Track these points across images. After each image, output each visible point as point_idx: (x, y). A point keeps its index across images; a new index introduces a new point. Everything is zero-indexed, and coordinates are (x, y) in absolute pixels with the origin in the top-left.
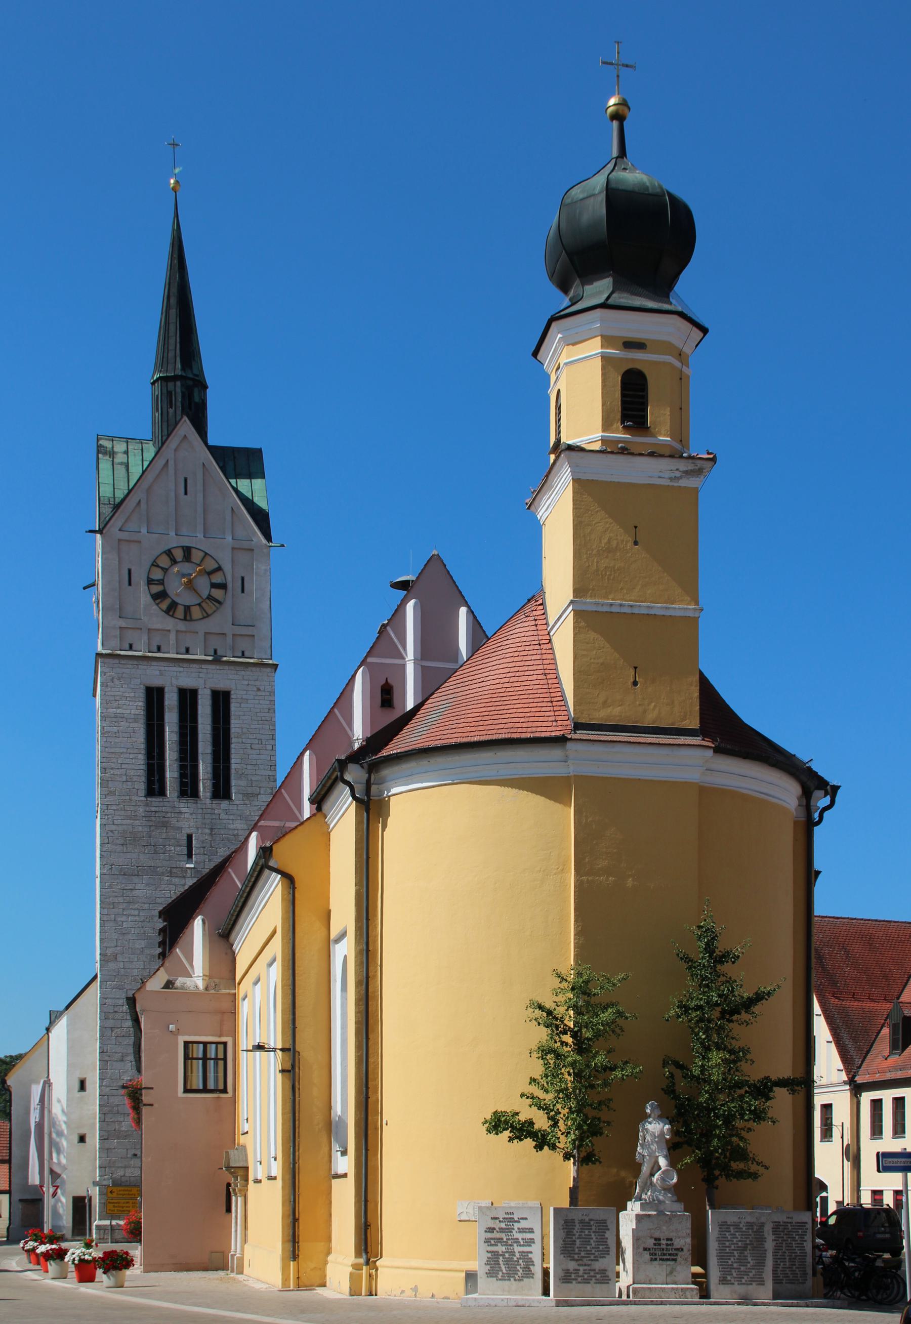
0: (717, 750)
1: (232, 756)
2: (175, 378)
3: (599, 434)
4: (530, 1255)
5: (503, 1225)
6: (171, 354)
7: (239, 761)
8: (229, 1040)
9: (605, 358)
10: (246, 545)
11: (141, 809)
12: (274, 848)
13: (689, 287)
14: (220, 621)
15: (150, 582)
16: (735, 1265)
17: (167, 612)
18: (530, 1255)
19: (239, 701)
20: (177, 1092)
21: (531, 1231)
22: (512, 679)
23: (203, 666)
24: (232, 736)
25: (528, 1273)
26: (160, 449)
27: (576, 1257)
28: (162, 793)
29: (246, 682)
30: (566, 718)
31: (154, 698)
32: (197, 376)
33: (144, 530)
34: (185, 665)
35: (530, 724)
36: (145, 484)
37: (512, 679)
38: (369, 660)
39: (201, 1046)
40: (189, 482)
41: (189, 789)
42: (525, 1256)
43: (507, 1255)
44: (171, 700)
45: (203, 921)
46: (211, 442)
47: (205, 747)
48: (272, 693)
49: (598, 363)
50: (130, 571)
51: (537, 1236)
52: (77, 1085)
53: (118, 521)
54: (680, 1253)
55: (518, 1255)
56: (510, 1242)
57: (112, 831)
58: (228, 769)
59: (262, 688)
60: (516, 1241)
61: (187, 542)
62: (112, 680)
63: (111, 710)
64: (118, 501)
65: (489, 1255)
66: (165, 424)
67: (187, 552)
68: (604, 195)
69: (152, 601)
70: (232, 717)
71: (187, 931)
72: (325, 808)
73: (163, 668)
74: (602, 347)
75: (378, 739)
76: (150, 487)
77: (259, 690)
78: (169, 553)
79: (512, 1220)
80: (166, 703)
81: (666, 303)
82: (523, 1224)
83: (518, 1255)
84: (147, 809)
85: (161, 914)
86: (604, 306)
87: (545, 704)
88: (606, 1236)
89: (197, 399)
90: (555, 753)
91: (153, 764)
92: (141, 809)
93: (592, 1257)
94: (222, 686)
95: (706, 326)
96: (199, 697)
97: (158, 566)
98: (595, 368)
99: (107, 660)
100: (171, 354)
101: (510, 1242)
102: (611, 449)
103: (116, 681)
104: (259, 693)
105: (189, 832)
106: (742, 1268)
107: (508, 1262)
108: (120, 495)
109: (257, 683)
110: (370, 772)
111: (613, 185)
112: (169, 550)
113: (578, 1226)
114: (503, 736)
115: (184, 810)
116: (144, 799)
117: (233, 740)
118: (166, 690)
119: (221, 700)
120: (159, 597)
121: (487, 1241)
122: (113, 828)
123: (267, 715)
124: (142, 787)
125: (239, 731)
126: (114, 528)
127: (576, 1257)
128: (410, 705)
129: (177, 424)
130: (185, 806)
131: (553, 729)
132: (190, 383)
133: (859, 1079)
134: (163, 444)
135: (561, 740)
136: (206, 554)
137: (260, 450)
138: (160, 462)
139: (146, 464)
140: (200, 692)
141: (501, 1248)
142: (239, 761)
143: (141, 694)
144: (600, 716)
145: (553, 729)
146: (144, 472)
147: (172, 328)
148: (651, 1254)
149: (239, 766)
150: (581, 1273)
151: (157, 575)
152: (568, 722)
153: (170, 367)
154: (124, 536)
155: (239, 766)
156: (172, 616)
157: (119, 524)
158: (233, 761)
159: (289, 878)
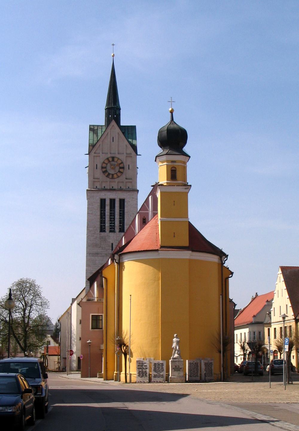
1: (125, 219)
3: (166, 181)
5: (141, 365)
6: (111, 101)
9: (167, 165)
13: (186, 149)
15: (102, 168)
17: (107, 176)
20: (89, 329)
21: (146, 366)
24: (125, 212)
25: (146, 375)
27: (157, 372)
28: (105, 231)
29: (129, 196)
31: (103, 201)
32: (117, 107)
33: (101, 153)
36: (102, 140)
38: (140, 212)
41: (112, 230)
44: (108, 202)
47: (117, 216)
53: (93, 151)
57: (90, 243)
59: (134, 198)
61: (113, 155)
63: (90, 206)
66: (108, 121)
67: (113, 158)
68: (166, 131)
73: (105, 193)
77: (133, 198)
78: (108, 159)
79: (143, 364)
80: (106, 203)
82: (145, 365)
83: (144, 371)
89: (117, 113)
90: (155, 253)
91: (102, 222)
94: (122, 197)
95: (190, 156)
98: (165, 167)
99: (90, 192)
102: (169, 185)
103: (92, 197)
105: (112, 242)
108: (95, 143)
109: (133, 196)
113: (157, 365)
114: (145, 249)
115: (110, 236)
116: (99, 233)
117: (125, 214)
118: (106, 199)
119: (122, 202)
120: (104, 172)
122: (90, 242)
124: (99, 230)
127: (157, 372)
130: (112, 234)
134: (108, 127)
135: (157, 250)
138: (106, 133)
139: (103, 133)
140: (116, 200)
141: (140, 370)
143: (99, 201)
144: (165, 245)
146: (102, 135)
147: (111, 94)
151: (104, 165)
154: (96, 155)
158: (125, 220)
159: (105, 278)
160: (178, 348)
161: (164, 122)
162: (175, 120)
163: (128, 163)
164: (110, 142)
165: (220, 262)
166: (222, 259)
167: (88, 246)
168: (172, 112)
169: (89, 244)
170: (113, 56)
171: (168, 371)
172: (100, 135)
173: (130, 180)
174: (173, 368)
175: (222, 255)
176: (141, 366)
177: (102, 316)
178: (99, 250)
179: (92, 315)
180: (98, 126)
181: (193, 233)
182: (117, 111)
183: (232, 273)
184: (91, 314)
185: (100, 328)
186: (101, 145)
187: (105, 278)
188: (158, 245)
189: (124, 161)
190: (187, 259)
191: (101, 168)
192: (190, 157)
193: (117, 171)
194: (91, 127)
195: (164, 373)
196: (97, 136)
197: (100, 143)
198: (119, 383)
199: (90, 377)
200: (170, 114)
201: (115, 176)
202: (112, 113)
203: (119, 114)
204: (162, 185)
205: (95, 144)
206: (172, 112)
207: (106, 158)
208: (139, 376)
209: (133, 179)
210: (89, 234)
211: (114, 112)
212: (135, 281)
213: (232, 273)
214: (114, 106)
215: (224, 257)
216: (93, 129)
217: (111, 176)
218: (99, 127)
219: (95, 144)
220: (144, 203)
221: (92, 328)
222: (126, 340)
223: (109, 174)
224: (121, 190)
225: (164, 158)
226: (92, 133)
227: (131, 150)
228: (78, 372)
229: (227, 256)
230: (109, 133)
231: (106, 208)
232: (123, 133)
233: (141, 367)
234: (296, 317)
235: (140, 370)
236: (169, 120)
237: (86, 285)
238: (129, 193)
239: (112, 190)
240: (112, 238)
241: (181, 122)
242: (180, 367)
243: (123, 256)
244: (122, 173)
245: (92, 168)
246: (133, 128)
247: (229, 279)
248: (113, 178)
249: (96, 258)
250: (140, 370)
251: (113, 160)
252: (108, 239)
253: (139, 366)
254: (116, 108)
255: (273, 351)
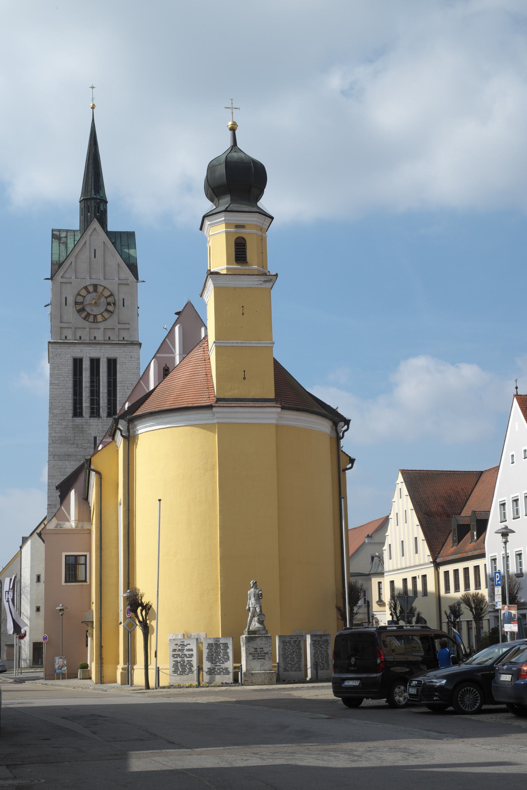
0: (283, 408)
1: (118, 393)
2: (91, 199)
4: (192, 662)
5: (180, 648)
7: (121, 396)
8: (88, 554)
9: (227, 233)
10: (125, 282)
11: (70, 424)
12: (92, 459)
14: (112, 322)
15: (76, 303)
16: (290, 662)
17: (85, 319)
18: (192, 662)
19: (122, 364)
22: (192, 377)
23: (103, 346)
24: (118, 383)
25: (191, 671)
26: (83, 234)
27: (214, 662)
29: (125, 354)
30: (213, 396)
31: (77, 363)
33: (73, 277)
34: (94, 346)
35: (197, 399)
37: (192, 377)
38: (157, 355)
39: (74, 557)
40: (96, 251)
41: (95, 413)
42: (189, 662)
43: (182, 662)
44: (86, 365)
45: (75, 491)
46: (110, 228)
48: (138, 359)
49: (224, 235)
50: (66, 298)
51: (195, 652)
52: (35, 578)
53: (61, 273)
54: (267, 655)
55: (186, 662)
56: (183, 656)
57: (55, 437)
58: (115, 400)
59: (133, 357)
60: (185, 655)
61: (95, 282)
62: (56, 356)
63: (55, 372)
64: (61, 262)
65: (174, 663)
66: (86, 223)
67: (95, 286)
68: (224, 165)
69: (77, 313)
70: (118, 373)
71: (67, 498)
72: (115, 438)
74: (226, 228)
75: (135, 407)
76: (77, 254)
77: (132, 357)
78: (86, 288)
80: (84, 366)
81: (253, 206)
82: (189, 647)
83: (186, 662)
84: (73, 423)
85: (57, 488)
86: (226, 211)
87: (205, 389)
88: (228, 651)
89: (102, 208)
92: (70, 424)
93: (221, 662)
94: (112, 355)
95: (273, 215)
96: (101, 362)
97: (80, 295)
98: (222, 238)
99: (54, 345)
100: (90, 187)
101: (183, 656)
103: (58, 356)
104: (132, 359)
105: (95, 435)
106: (293, 663)
107: (182, 665)
108: (62, 259)
109: (131, 354)
110: (129, 423)
111: (228, 160)
112: (86, 287)
115: (92, 424)
116: (71, 418)
117: (118, 385)
118: (84, 360)
119: (112, 363)
120: (79, 311)
121: (173, 656)
122: (55, 435)
123: (136, 370)
125: (121, 379)
126: (58, 277)
127: (214, 662)
128: (152, 387)
129: (92, 221)
130: (94, 421)
131: (207, 401)
132: (98, 201)
133: (438, 560)
134: (85, 231)
135: (210, 407)
136: (105, 288)
137: (134, 232)
138: (82, 242)
139: (76, 242)
140: (101, 360)
141: (179, 659)
142: (121, 396)
143: (71, 363)
144: (228, 395)
145: (207, 401)
146: (75, 246)
147: (90, 174)
148: (253, 656)
149: (121, 399)
150: (216, 670)
151: (80, 299)
152: (214, 398)
153: (89, 193)
154: (64, 280)
155: (121, 399)
156: (87, 321)
157: (61, 274)
158: (118, 396)
159: (98, 473)
160: (258, 610)
161: (220, 147)
162: (239, 145)
163: (122, 296)
164: (90, 259)
165: (334, 435)
166: (338, 428)
167: (52, 442)
168: (233, 129)
169: (54, 438)
170: (93, 108)
171: (237, 658)
172: (71, 246)
173: (127, 326)
174: (250, 654)
175: (337, 420)
176: (179, 650)
177: (86, 556)
178: (71, 450)
179: (66, 556)
180: (67, 231)
181: (282, 376)
182: (101, 204)
183: (352, 461)
184: (64, 554)
185: (81, 580)
186: (73, 264)
187: (98, 473)
188: (211, 396)
189: (116, 293)
190: (274, 424)
191: (74, 304)
192: (272, 218)
193: (102, 309)
194: (54, 233)
195: (230, 665)
196: (66, 247)
197: (72, 259)
198: (133, 688)
199: (62, 679)
200: (230, 133)
201: (100, 318)
202: (93, 209)
203: (105, 211)
204: (217, 273)
205: (63, 262)
206: (233, 129)
207: (83, 285)
208: (175, 672)
209: (130, 324)
210: (53, 421)
211: (95, 206)
212: (167, 471)
213: (352, 461)
214: (95, 197)
215: (342, 424)
216: (57, 236)
217: (91, 319)
218: (69, 234)
219: (63, 262)
220: (165, 339)
221: (66, 582)
222: (148, 597)
223: (88, 315)
224: (108, 343)
225: (222, 218)
226: (58, 243)
227: (126, 272)
228: (33, 671)
229: (347, 422)
230: (88, 242)
231: (84, 376)
232: (114, 243)
233: (180, 653)
234: (436, 559)
235: (176, 659)
236: (228, 144)
237: (48, 512)
238: (123, 349)
239: (94, 343)
240: (94, 427)
241: (251, 148)
242: (266, 650)
243: (136, 423)
244: (112, 313)
245: (58, 305)
246: (131, 235)
247: (347, 472)
248: (95, 321)
249: (67, 463)
250: (176, 659)
251: (95, 290)
252: (87, 429)
253: (174, 650)
254: (100, 199)
255: (496, 608)
